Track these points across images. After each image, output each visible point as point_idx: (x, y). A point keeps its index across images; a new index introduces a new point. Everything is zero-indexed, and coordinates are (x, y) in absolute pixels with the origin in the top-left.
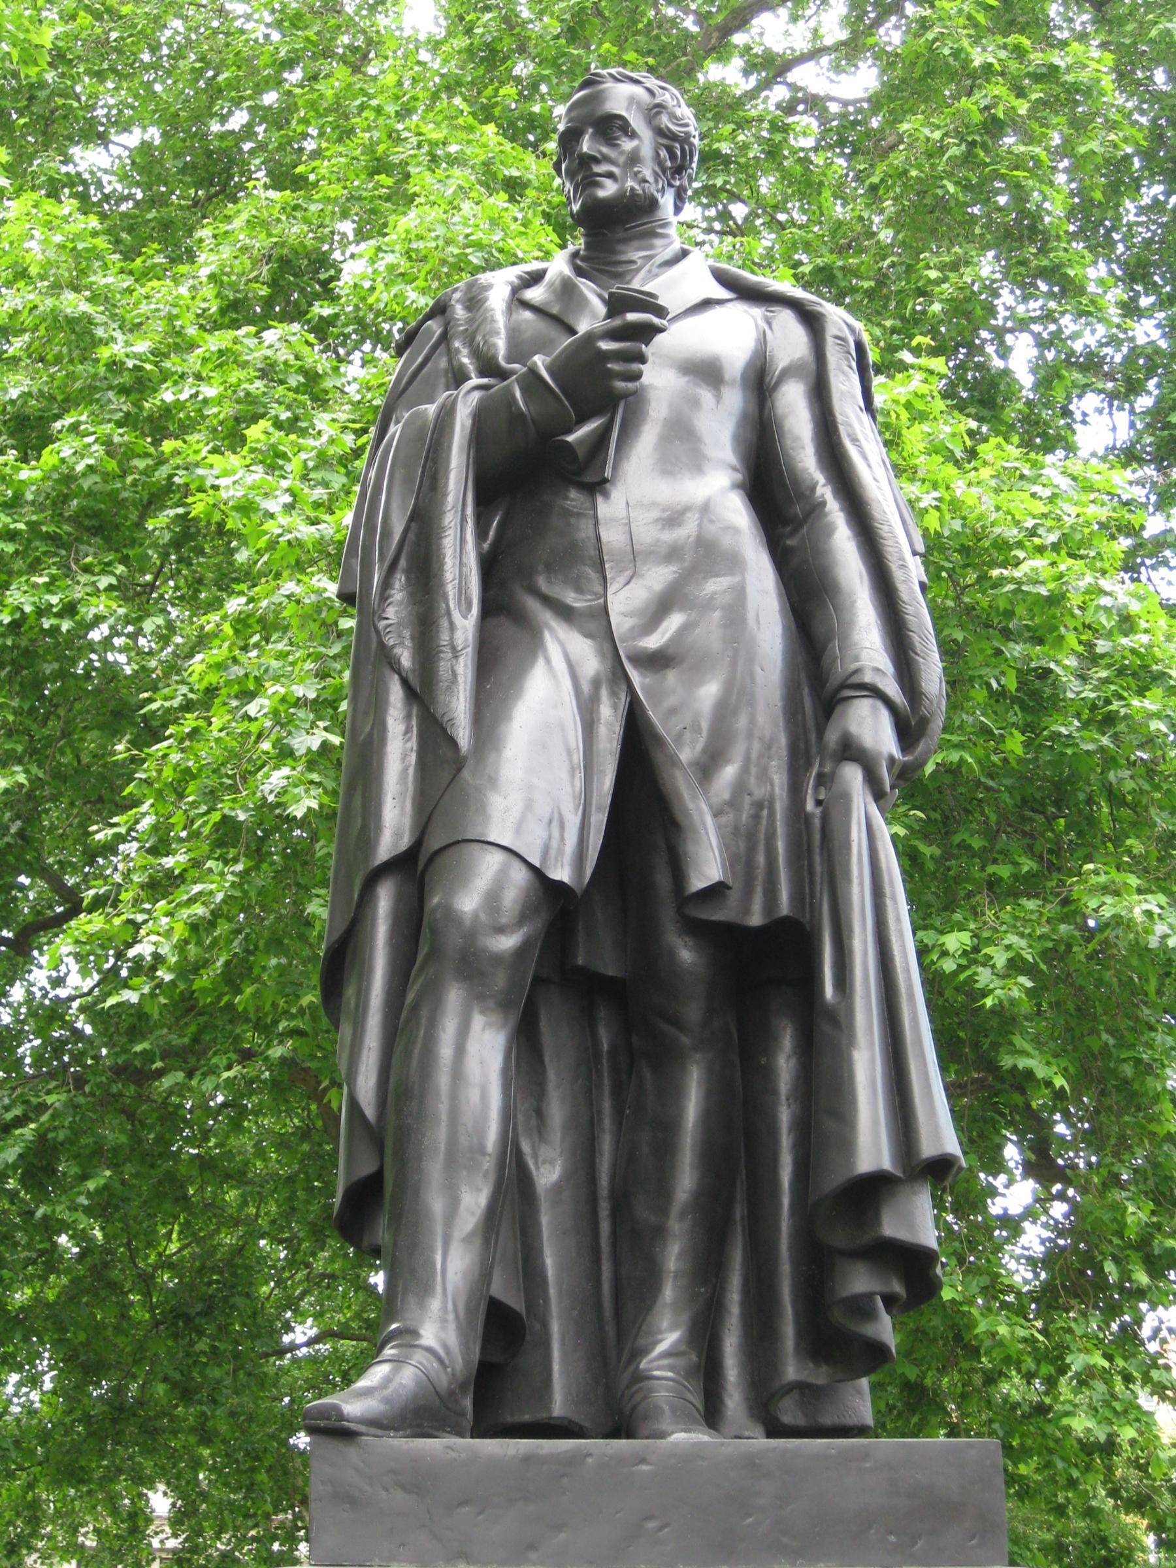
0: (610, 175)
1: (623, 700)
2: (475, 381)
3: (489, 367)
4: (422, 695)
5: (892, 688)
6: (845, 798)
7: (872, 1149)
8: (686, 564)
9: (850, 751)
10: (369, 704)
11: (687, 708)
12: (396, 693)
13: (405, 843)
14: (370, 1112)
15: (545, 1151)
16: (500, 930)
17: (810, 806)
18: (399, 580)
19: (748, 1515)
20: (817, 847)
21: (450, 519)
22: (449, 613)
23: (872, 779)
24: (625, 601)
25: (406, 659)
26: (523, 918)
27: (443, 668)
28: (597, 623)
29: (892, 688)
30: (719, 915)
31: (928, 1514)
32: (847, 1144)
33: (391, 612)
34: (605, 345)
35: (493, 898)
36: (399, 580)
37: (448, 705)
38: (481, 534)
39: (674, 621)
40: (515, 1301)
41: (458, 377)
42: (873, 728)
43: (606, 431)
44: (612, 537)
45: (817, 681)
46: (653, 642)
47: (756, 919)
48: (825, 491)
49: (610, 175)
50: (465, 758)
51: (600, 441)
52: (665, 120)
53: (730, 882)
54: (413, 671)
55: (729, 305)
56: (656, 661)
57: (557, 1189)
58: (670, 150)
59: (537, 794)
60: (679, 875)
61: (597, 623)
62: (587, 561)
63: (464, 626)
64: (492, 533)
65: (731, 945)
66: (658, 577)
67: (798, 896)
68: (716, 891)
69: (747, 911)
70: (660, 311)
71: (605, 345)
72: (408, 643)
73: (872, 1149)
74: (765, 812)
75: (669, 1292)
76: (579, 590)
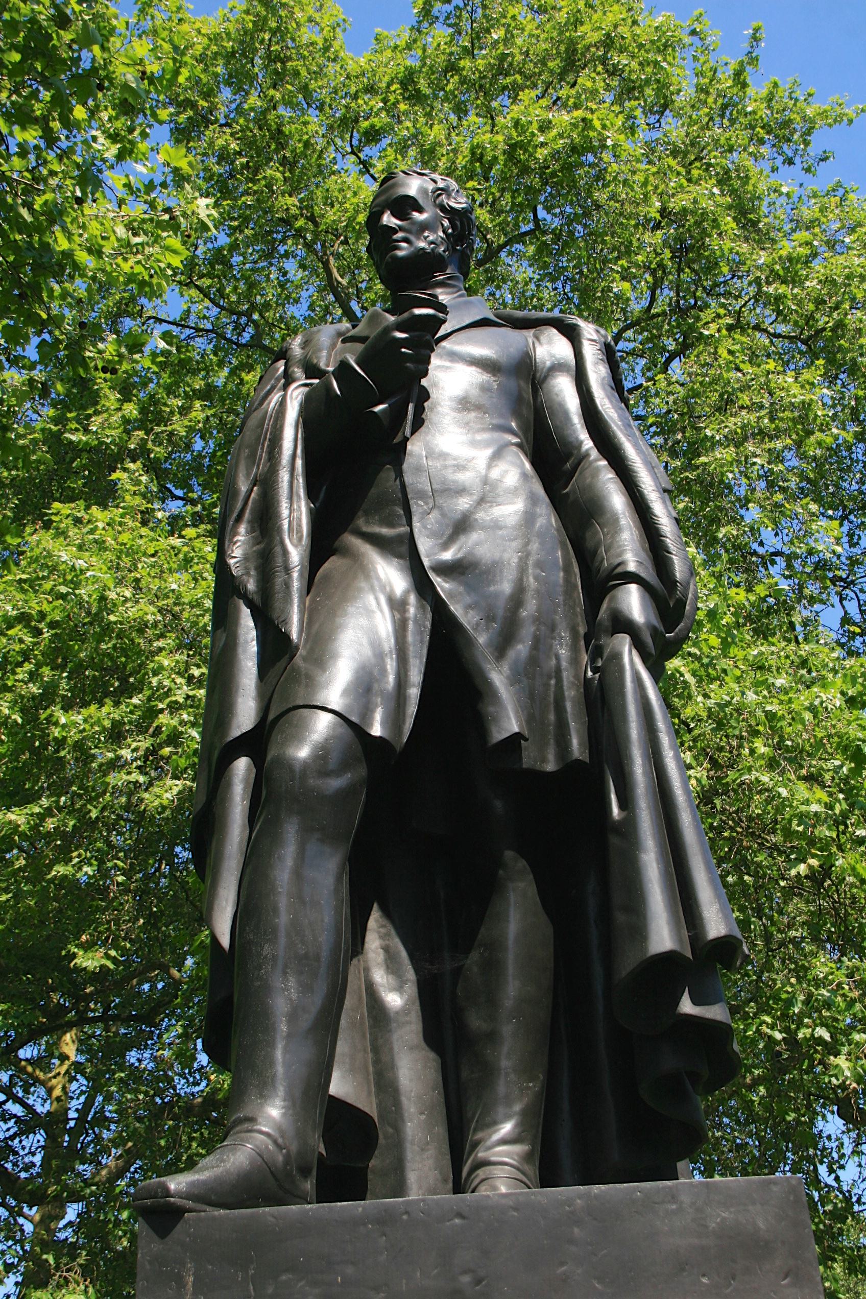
3: (312, 370)
6: (616, 657)
7: (662, 936)
8: (475, 497)
10: (223, 617)
14: (225, 942)
19: (562, 1264)
22: (282, 543)
23: (638, 644)
25: (251, 586)
31: (740, 1251)
32: (639, 930)
37: (283, 611)
40: (368, 1104)
41: (288, 379)
42: (633, 602)
47: (550, 766)
50: (297, 648)
53: (526, 733)
54: (256, 593)
55: (503, 329)
61: (406, 551)
64: (322, 495)
69: (544, 760)
72: (252, 573)
73: (662, 936)
74: (553, 682)
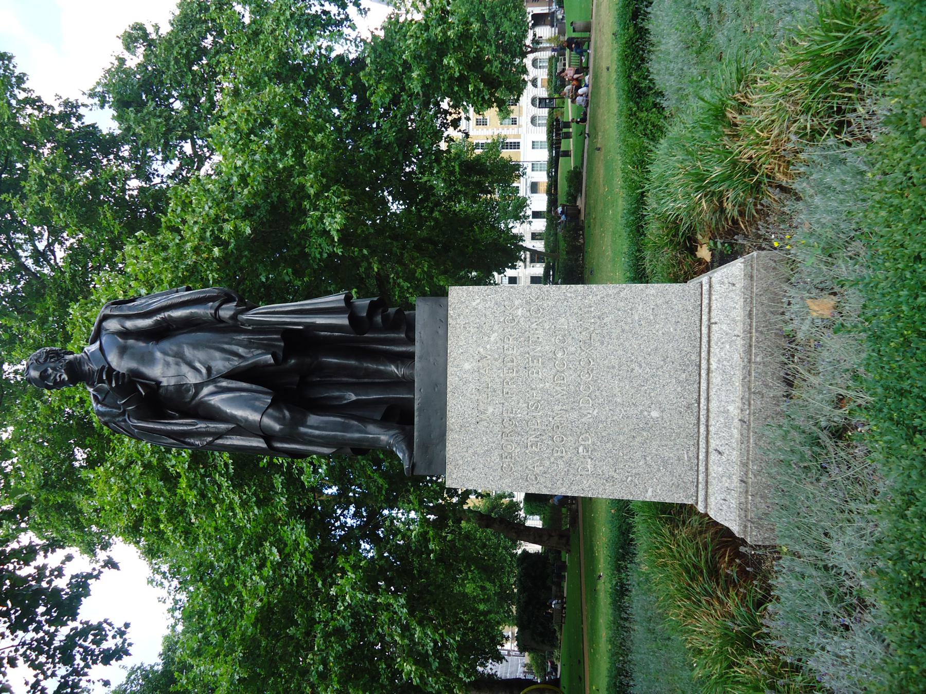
0: (60, 376)
1: (221, 379)
2: (126, 417)
3: (123, 414)
4: (220, 435)
5: (217, 304)
7: (343, 321)
9: (234, 317)
11: (220, 364)
12: (220, 441)
13: (262, 440)
15: (347, 397)
16: (284, 416)
17: (250, 328)
18: (188, 440)
20: (261, 328)
21: (169, 428)
24: (192, 378)
25: (211, 439)
26: (281, 411)
27: (212, 430)
28: (199, 387)
29: (217, 304)
30: (281, 354)
33: (197, 443)
34: (114, 385)
35: (276, 419)
36: (188, 440)
38: (173, 418)
39: (198, 365)
40: (383, 408)
42: (226, 312)
43: (142, 384)
44: (173, 382)
45: (215, 325)
46: (204, 371)
47: (282, 344)
48: (158, 317)
49: (60, 376)
51: (144, 386)
52: (41, 360)
56: (209, 369)
57: (356, 395)
58: (52, 358)
59: (245, 408)
60: (271, 365)
62: (181, 389)
63: (201, 426)
65: (288, 352)
66: (185, 369)
67: (275, 332)
68: (274, 356)
70: (103, 368)
71: (114, 385)
75: (382, 368)
76: (189, 390)
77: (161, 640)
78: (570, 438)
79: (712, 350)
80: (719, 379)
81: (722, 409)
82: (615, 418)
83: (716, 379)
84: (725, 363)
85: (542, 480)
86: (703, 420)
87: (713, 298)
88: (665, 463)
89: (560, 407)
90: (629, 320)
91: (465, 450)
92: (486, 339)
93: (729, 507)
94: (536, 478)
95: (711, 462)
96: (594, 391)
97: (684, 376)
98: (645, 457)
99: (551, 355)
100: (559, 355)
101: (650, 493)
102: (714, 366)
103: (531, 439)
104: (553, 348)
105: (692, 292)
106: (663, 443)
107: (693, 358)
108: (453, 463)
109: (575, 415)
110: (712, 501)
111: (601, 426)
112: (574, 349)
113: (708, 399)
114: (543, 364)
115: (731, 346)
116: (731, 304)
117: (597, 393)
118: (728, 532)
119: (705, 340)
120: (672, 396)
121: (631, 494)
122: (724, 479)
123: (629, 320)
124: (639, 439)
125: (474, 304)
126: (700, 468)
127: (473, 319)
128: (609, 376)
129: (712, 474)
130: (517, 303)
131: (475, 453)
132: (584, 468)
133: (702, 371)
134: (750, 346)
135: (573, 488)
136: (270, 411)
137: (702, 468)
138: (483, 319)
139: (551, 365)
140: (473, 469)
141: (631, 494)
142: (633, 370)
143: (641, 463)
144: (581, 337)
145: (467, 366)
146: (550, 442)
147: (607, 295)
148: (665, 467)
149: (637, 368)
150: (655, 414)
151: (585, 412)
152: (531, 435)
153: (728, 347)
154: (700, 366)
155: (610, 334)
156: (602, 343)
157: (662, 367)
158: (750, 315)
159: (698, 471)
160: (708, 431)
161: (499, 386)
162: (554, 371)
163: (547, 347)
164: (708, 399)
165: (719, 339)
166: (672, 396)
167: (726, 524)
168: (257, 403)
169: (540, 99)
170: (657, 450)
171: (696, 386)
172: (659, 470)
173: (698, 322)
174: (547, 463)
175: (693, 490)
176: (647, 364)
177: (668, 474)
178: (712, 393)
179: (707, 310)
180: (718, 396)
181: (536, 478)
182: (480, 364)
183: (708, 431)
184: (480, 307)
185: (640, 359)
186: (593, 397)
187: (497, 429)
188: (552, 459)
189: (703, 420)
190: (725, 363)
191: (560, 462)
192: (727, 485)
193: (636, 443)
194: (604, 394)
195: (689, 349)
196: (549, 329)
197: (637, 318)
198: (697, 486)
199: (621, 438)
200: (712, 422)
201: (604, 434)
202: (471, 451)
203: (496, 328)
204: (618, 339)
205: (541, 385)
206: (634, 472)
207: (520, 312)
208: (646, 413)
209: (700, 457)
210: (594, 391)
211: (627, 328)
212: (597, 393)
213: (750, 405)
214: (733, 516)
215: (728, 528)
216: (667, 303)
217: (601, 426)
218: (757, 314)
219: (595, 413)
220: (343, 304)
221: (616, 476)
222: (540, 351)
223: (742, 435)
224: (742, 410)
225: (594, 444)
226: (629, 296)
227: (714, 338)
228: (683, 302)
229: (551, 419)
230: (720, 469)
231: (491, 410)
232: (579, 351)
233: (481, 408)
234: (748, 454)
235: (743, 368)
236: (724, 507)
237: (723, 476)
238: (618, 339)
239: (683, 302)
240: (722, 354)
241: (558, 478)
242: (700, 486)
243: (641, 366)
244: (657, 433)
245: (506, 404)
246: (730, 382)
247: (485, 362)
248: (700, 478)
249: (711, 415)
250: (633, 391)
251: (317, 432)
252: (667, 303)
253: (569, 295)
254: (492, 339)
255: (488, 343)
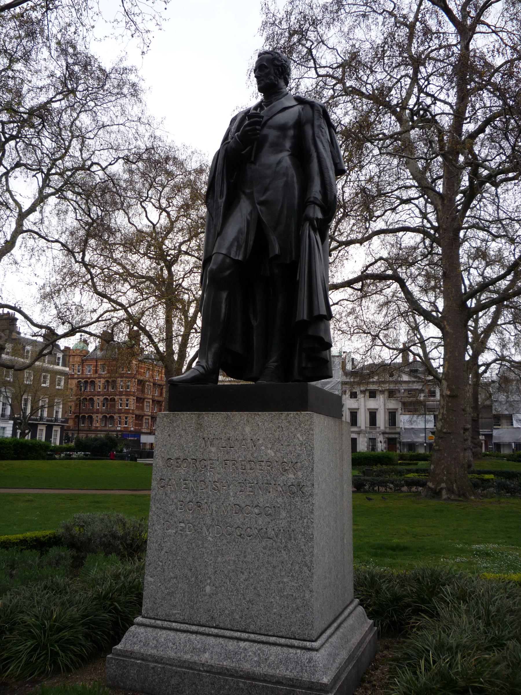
47: (288, 262)
77: (261, 22)
78: (191, 516)
79: (255, 644)
80: (231, 648)
81: (207, 647)
82: (206, 555)
83: (231, 645)
84: (243, 655)
85: (161, 492)
86: (202, 629)
87: (299, 651)
88: (171, 594)
89: (214, 509)
90: (283, 573)
91: (184, 428)
92: (270, 446)
93: (135, 644)
94: (162, 487)
95: (169, 632)
96: (226, 539)
97: (237, 617)
98: (176, 578)
99: (256, 503)
100: (256, 511)
101: (150, 579)
102: (242, 644)
103: (191, 484)
104: (261, 505)
105: (307, 632)
106: (186, 594)
107: (252, 626)
108: (174, 418)
109: (209, 521)
110: (142, 630)
111: (200, 542)
112: (260, 523)
113: (216, 636)
114: (249, 495)
115: (256, 662)
116: (291, 667)
117: (225, 541)
118: (118, 641)
119: (264, 638)
120: (221, 605)
121: (149, 564)
122: (155, 642)
123: (283, 573)
124: (189, 574)
125: (299, 435)
126: (166, 623)
127: (286, 434)
128: (238, 553)
129: (160, 632)
130: (299, 473)
131: (181, 436)
132: (168, 526)
133: (239, 634)
134: (254, 679)
135: (155, 517)
136: (228, 260)
137: (166, 624)
138: (286, 444)
139: (248, 503)
140: (169, 435)
141: (149, 564)
142: (243, 573)
143: (171, 574)
144: (270, 530)
145: (248, 429)
146: (188, 499)
147: (305, 555)
148: (168, 594)
149: (244, 577)
150: (208, 589)
151: (210, 530)
152: (194, 484)
153: (256, 659)
154: (244, 632)
155: (272, 555)
156: (264, 548)
157: (244, 599)
158: (278, 683)
159: (165, 620)
160: (193, 632)
161: (231, 458)
162: (243, 505)
163: (262, 500)
164: (216, 636)
165: (263, 652)
166: (221, 605)
167: (123, 640)
168: (234, 249)
169: (354, 524)
170: (181, 588)
171: (229, 626)
172: (166, 588)
173: (280, 634)
174: (173, 496)
175: (151, 615)
176: (247, 586)
177: (164, 595)
178: (221, 640)
179: (289, 644)
180: (218, 645)
181: (162, 487)
182: (249, 441)
183: (193, 632)
184: (296, 440)
185: (252, 580)
186: (222, 538)
187: (199, 455)
188: (175, 500)
189: (202, 629)
190: (243, 655)
191: (173, 507)
192: (151, 644)
193: (186, 571)
194: (224, 548)
195: (258, 623)
196: (277, 502)
197: (285, 580)
198: (154, 619)
199: (190, 559)
200: (199, 637)
201: (194, 544)
202: (183, 433)
203: (279, 455)
204: (268, 562)
205: (232, 494)
206: (166, 568)
207: (291, 476)
208: (209, 581)
209: (174, 624)
210: (226, 539)
211: (277, 571)
212: (225, 541)
213: (207, 672)
214: (129, 648)
215: (120, 641)
216: (297, 609)
217: (200, 542)
218: (278, 689)
219: (209, 538)
220: (316, 313)
221: (163, 552)
222: (259, 494)
223: (185, 661)
224: (203, 664)
225: (187, 536)
226: (303, 574)
227: (265, 648)
228: (298, 623)
229: (205, 501)
230: (163, 640)
231: (213, 449)
232: (259, 528)
233: (216, 442)
234: (170, 665)
235: (235, 670)
236: (139, 639)
237: (157, 641)
238: (268, 562)
239: (298, 623)
240: (250, 653)
241: (162, 505)
242: (153, 621)
243: (246, 580)
244: (194, 589)
245: (218, 463)
246: (226, 658)
247: (250, 444)
248: (159, 622)
249: (204, 637)
250: (226, 572)
251: (307, 246)
252: (297, 609)
253: (305, 521)
254: (269, 451)
255: (266, 447)
